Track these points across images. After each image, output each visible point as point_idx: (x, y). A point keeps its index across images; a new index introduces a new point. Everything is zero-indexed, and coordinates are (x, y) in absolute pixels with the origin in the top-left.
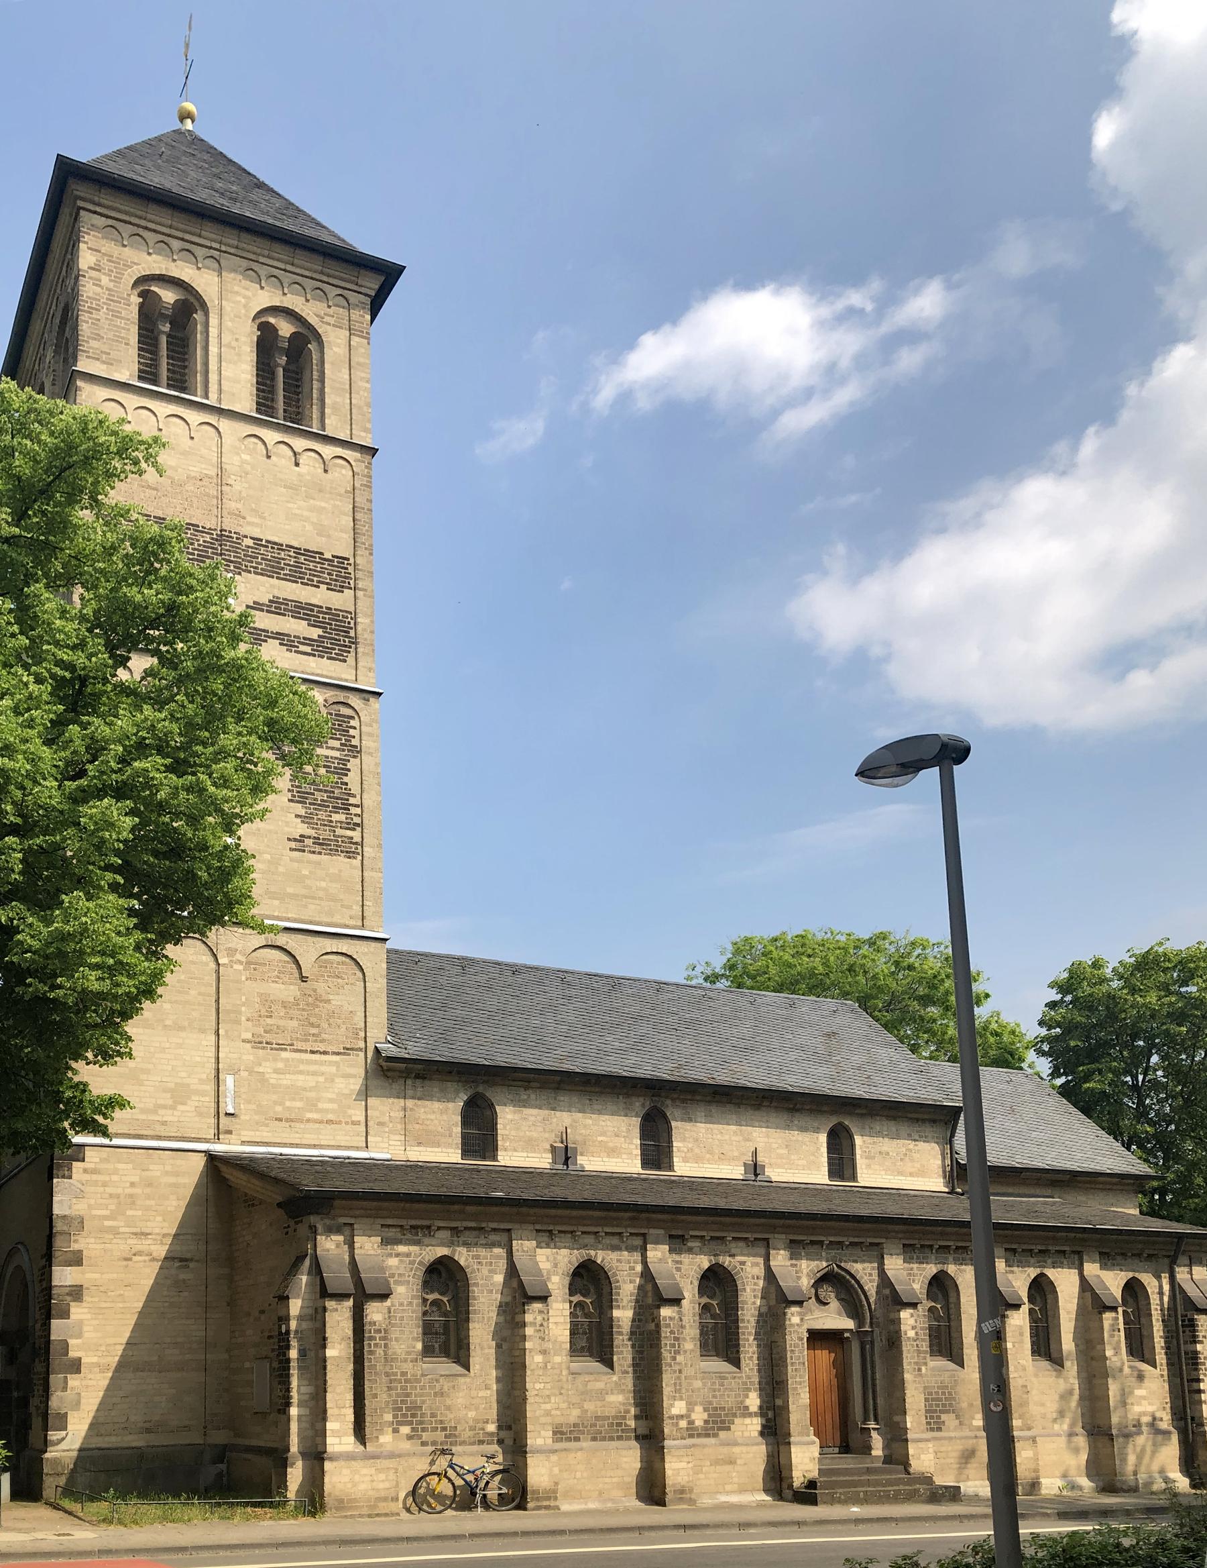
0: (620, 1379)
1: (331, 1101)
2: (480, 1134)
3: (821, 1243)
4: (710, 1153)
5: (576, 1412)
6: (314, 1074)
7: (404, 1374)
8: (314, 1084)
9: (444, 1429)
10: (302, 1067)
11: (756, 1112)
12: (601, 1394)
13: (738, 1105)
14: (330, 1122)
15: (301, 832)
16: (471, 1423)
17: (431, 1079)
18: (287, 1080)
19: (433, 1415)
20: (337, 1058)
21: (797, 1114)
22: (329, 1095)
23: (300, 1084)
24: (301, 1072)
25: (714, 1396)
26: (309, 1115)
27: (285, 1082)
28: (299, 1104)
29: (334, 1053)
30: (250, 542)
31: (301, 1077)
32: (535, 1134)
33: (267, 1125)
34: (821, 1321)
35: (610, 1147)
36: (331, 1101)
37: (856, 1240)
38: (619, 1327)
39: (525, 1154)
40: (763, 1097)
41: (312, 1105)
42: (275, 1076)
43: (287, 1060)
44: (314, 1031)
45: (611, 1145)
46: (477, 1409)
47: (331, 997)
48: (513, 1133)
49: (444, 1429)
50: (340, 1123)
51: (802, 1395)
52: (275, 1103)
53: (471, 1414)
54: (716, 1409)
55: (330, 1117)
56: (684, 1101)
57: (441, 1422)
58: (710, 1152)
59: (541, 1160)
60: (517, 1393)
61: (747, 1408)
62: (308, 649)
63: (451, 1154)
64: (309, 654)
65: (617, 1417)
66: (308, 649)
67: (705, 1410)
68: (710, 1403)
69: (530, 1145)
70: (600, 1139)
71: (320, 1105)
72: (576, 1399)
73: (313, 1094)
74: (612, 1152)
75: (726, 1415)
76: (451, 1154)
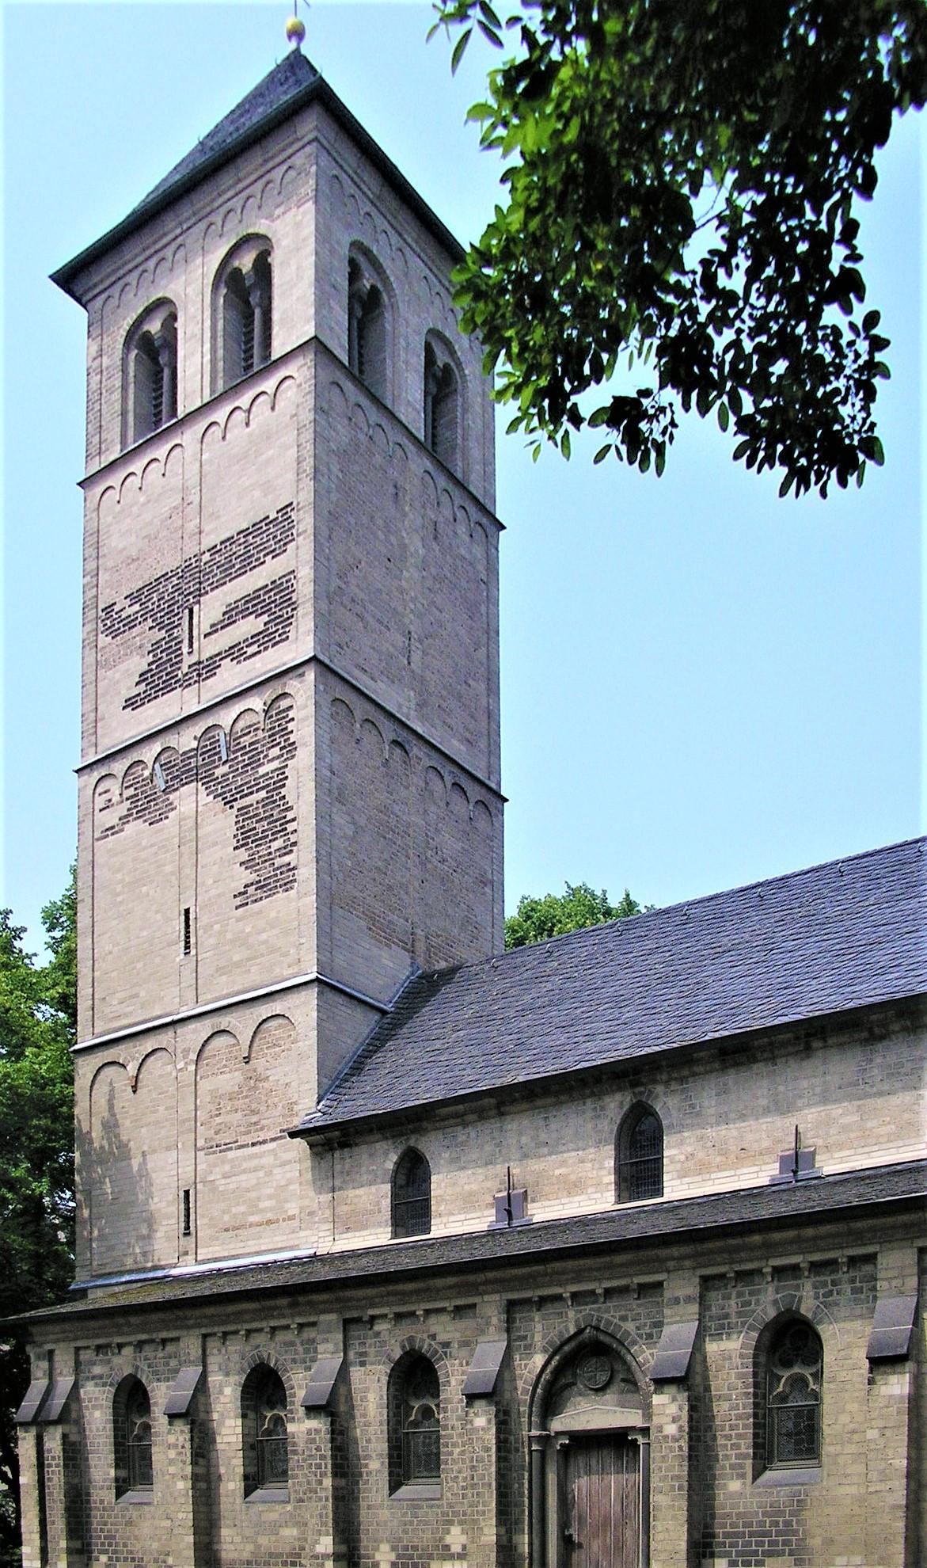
0: (295, 1508)
1: (270, 1197)
2: (411, 1206)
3: (558, 1298)
4: (717, 1159)
5: (250, 1547)
6: (255, 1170)
7: (102, 1502)
8: (255, 1181)
9: (133, 1559)
10: (245, 1165)
11: (804, 1063)
12: (275, 1528)
13: (773, 1059)
14: (270, 1222)
15: (245, 881)
16: (156, 1555)
17: (356, 1145)
18: (233, 1183)
19: (125, 1545)
20: (273, 1145)
21: (879, 1046)
22: (269, 1191)
23: (244, 1184)
24: (244, 1172)
25: (405, 1532)
26: (252, 1219)
27: (231, 1186)
28: (242, 1209)
29: (273, 1140)
30: (206, 557)
31: (243, 1177)
32: (474, 1187)
33: (217, 1239)
34: (584, 1418)
35: (574, 1184)
36: (270, 1197)
37: (615, 1283)
38: (294, 1444)
39: (462, 1217)
40: (808, 1035)
41: (254, 1208)
42: (223, 1181)
43: (232, 1160)
44: (254, 1119)
45: (573, 1177)
46: (160, 1540)
47: (268, 1073)
48: (449, 1191)
49: (133, 1559)
50: (277, 1221)
51: (486, 1531)
52: (224, 1212)
53: (155, 1545)
54: (406, 1548)
55: (269, 1216)
56: (682, 1080)
57: (131, 1552)
58: (723, 1153)
59: (481, 1220)
60: (203, 1524)
61: (447, 1547)
62: (254, 648)
63: (380, 1236)
64: (259, 652)
65: (290, 1555)
66: (254, 648)
67: (393, 1549)
68: (400, 1540)
69: (468, 1202)
70: (557, 1172)
71: (262, 1205)
72: (248, 1532)
73: (254, 1194)
74: (574, 1187)
75: (420, 1557)
76: (380, 1236)
